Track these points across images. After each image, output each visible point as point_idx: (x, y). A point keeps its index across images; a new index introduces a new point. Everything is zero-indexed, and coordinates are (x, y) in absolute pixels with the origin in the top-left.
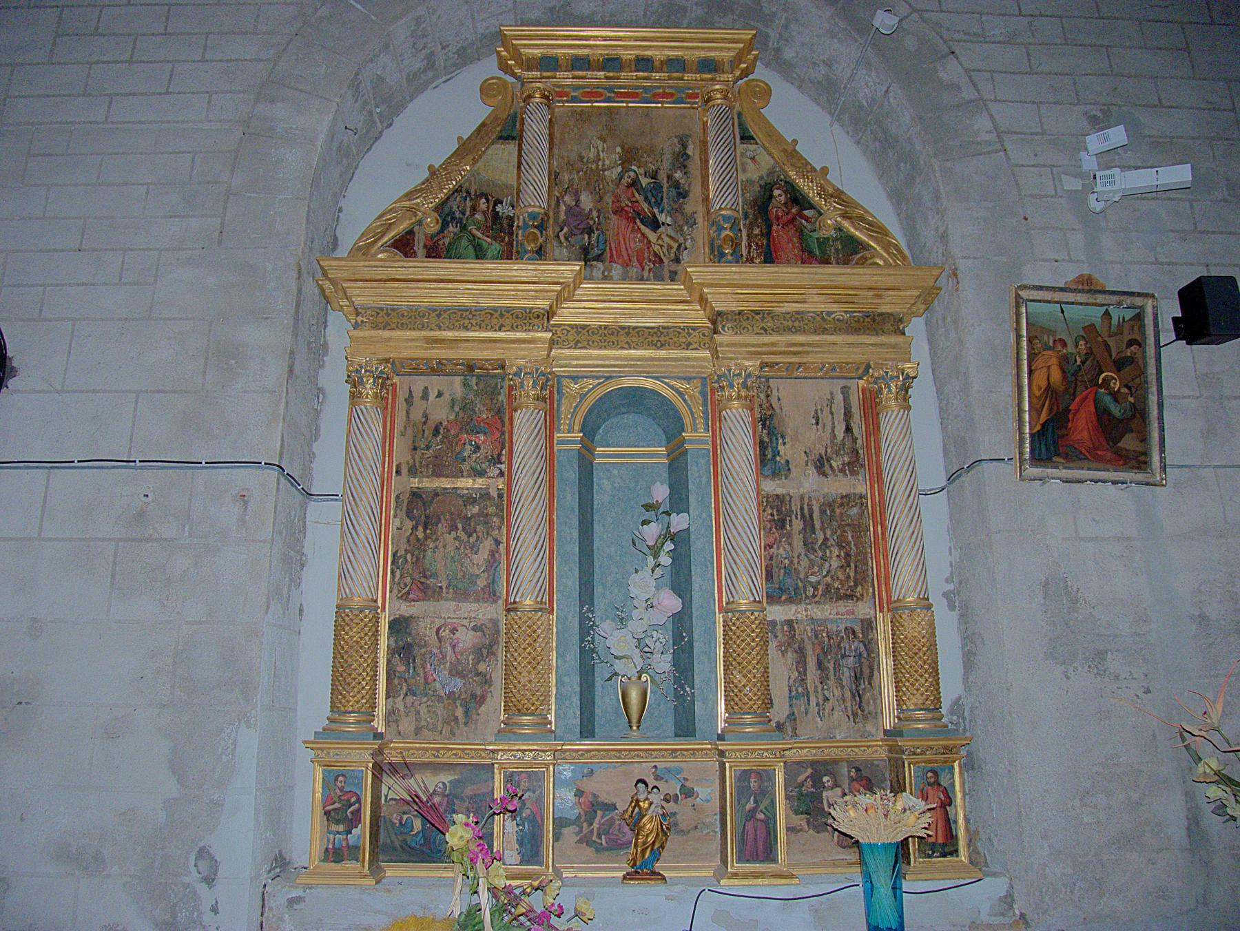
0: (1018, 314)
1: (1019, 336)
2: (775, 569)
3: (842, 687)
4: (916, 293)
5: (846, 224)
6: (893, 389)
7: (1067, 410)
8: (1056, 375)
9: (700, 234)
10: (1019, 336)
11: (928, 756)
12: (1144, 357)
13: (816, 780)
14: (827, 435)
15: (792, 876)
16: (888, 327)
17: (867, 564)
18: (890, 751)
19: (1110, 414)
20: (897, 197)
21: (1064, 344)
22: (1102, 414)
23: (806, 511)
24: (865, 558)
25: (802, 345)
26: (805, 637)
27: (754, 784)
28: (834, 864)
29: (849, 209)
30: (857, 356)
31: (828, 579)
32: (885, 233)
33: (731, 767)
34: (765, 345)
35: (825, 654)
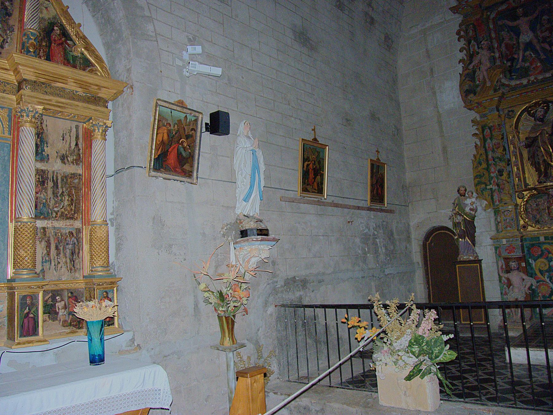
0: (156, 110)
1: (155, 119)
2: (39, 204)
3: (66, 257)
4: (115, 92)
5: (86, 53)
6: (101, 131)
7: (168, 151)
8: (166, 137)
9: (15, 37)
10: (155, 119)
11: (105, 286)
12: (196, 136)
13: (53, 298)
14: (68, 145)
15: (46, 341)
16: (101, 103)
17: (80, 204)
18: (86, 285)
19: (182, 155)
20: (107, 46)
21: (170, 126)
22: (179, 154)
23: (55, 179)
24: (80, 202)
25: (63, 103)
26: (51, 235)
27: (28, 301)
28: (60, 334)
29: (88, 46)
30: (87, 113)
31: (63, 210)
32: (103, 62)
33: (18, 294)
34: (46, 100)
35: (59, 243)
